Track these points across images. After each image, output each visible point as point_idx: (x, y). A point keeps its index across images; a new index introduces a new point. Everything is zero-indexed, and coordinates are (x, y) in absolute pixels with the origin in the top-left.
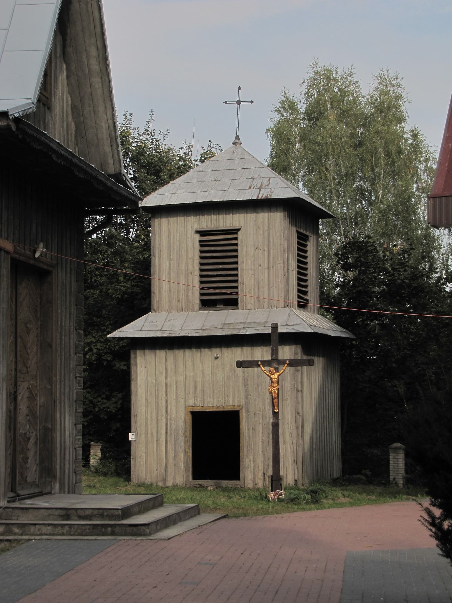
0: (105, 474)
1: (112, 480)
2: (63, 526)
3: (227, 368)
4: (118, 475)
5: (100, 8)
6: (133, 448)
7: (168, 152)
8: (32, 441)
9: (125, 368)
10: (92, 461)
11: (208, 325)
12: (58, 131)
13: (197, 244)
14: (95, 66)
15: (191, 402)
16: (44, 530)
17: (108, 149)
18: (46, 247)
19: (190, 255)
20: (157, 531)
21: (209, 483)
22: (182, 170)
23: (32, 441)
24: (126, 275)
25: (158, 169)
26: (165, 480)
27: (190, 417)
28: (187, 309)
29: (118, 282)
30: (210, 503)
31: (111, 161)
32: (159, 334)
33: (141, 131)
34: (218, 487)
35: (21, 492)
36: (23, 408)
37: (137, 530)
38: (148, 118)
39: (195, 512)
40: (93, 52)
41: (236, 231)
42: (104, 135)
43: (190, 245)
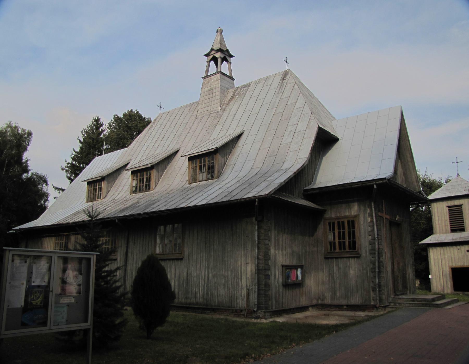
0: (422, 289)
1: (425, 291)
2: (412, 304)
3: (463, 253)
4: (426, 289)
5: (409, 142)
6: (431, 281)
7: (433, 181)
8: (399, 277)
9: (425, 254)
10: (417, 285)
11: (454, 238)
12: (400, 181)
13: (448, 211)
14: (409, 160)
15: (451, 264)
16: (407, 305)
17: (416, 184)
18: (399, 216)
19: (445, 214)
20: (445, 306)
21: (461, 293)
22: (440, 186)
23: (399, 277)
24: (423, 223)
25: (431, 186)
26: (443, 291)
27: (451, 270)
28: (446, 233)
29: (421, 225)
30: (462, 299)
31: (417, 188)
32: (437, 242)
33: (423, 175)
34: (464, 294)
35: (398, 293)
36: (396, 267)
37: (437, 306)
38: (425, 170)
39: (457, 301)
40: (408, 155)
41: (461, 205)
42: (414, 179)
43: (445, 211)
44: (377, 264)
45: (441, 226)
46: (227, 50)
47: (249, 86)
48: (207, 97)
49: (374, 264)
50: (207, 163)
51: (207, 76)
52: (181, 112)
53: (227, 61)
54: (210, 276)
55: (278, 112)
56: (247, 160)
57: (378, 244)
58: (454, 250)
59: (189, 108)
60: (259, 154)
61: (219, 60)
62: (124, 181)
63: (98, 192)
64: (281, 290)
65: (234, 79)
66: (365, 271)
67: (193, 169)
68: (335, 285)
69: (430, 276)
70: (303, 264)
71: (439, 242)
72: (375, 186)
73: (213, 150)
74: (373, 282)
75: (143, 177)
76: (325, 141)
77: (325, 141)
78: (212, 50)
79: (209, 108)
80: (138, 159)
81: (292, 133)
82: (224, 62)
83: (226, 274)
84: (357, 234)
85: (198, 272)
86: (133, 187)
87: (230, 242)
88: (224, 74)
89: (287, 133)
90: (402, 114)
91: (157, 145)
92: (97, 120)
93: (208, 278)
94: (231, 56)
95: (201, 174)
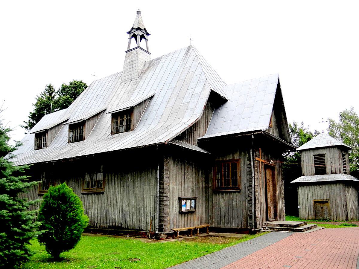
2: (281, 229)
8: (272, 208)
11: (318, 179)
15: (314, 198)
28: (312, 175)
44: (253, 197)
45: (308, 170)
46: (145, 29)
47: (161, 59)
48: (128, 68)
49: (251, 197)
50: (124, 119)
51: (129, 50)
52: (109, 80)
53: (145, 38)
54: (124, 205)
55: (181, 78)
56: (156, 116)
57: (255, 182)
58: (318, 189)
59: (116, 77)
60: (165, 111)
61: (139, 37)
62: (64, 134)
63: (43, 142)
64: (177, 217)
65: (150, 54)
66: (244, 203)
67: (115, 123)
68: (221, 213)
69: (299, 207)
70: (197, 196)
71: (306, 181)
72: (253, 136)
73: (130, 108)
74: (250, 211)
75: (78, 130)
76: (216, 102)
77: (216, 102)
78: (133, 28)
79: (130, 76)
80: (76, 116)
81: (191, 94)
82: (143, 39)
83: (136, 204)
84: (238, 174)
85: (115, 203)
86: (70, 137)
87: (139, 179)
88: (142, 49)
89: (187, 95)
90: (279, 81)
91: (90, 105)
92: (50, 88)
93: (122, 208)
94: (148, 34)
95: (121, 128)
